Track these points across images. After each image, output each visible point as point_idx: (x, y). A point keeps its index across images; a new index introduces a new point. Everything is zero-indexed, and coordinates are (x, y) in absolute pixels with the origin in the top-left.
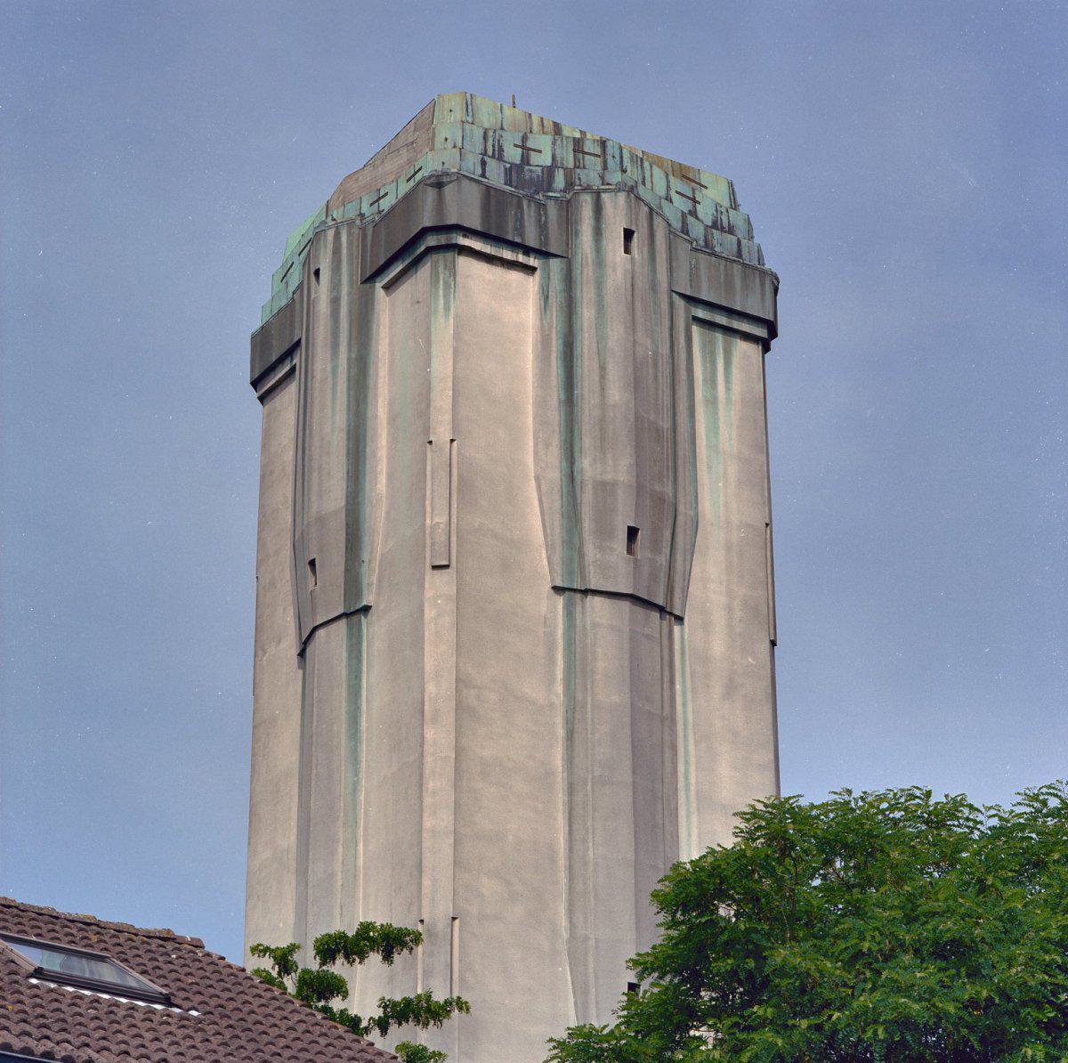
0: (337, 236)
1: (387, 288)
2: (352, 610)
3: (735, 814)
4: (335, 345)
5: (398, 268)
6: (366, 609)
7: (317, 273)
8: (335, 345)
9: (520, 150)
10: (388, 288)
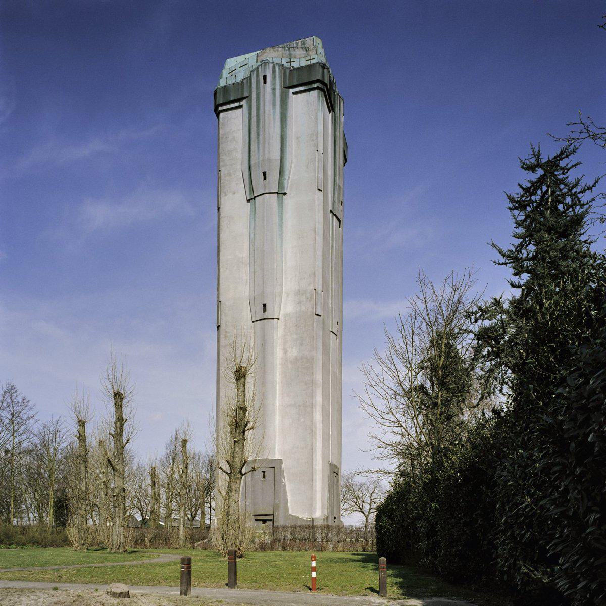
1: (294, 94)
4: (274, 105)
6: (285, 194)
7: (265, 77)
8: (274, 105)
10: (294, 94)
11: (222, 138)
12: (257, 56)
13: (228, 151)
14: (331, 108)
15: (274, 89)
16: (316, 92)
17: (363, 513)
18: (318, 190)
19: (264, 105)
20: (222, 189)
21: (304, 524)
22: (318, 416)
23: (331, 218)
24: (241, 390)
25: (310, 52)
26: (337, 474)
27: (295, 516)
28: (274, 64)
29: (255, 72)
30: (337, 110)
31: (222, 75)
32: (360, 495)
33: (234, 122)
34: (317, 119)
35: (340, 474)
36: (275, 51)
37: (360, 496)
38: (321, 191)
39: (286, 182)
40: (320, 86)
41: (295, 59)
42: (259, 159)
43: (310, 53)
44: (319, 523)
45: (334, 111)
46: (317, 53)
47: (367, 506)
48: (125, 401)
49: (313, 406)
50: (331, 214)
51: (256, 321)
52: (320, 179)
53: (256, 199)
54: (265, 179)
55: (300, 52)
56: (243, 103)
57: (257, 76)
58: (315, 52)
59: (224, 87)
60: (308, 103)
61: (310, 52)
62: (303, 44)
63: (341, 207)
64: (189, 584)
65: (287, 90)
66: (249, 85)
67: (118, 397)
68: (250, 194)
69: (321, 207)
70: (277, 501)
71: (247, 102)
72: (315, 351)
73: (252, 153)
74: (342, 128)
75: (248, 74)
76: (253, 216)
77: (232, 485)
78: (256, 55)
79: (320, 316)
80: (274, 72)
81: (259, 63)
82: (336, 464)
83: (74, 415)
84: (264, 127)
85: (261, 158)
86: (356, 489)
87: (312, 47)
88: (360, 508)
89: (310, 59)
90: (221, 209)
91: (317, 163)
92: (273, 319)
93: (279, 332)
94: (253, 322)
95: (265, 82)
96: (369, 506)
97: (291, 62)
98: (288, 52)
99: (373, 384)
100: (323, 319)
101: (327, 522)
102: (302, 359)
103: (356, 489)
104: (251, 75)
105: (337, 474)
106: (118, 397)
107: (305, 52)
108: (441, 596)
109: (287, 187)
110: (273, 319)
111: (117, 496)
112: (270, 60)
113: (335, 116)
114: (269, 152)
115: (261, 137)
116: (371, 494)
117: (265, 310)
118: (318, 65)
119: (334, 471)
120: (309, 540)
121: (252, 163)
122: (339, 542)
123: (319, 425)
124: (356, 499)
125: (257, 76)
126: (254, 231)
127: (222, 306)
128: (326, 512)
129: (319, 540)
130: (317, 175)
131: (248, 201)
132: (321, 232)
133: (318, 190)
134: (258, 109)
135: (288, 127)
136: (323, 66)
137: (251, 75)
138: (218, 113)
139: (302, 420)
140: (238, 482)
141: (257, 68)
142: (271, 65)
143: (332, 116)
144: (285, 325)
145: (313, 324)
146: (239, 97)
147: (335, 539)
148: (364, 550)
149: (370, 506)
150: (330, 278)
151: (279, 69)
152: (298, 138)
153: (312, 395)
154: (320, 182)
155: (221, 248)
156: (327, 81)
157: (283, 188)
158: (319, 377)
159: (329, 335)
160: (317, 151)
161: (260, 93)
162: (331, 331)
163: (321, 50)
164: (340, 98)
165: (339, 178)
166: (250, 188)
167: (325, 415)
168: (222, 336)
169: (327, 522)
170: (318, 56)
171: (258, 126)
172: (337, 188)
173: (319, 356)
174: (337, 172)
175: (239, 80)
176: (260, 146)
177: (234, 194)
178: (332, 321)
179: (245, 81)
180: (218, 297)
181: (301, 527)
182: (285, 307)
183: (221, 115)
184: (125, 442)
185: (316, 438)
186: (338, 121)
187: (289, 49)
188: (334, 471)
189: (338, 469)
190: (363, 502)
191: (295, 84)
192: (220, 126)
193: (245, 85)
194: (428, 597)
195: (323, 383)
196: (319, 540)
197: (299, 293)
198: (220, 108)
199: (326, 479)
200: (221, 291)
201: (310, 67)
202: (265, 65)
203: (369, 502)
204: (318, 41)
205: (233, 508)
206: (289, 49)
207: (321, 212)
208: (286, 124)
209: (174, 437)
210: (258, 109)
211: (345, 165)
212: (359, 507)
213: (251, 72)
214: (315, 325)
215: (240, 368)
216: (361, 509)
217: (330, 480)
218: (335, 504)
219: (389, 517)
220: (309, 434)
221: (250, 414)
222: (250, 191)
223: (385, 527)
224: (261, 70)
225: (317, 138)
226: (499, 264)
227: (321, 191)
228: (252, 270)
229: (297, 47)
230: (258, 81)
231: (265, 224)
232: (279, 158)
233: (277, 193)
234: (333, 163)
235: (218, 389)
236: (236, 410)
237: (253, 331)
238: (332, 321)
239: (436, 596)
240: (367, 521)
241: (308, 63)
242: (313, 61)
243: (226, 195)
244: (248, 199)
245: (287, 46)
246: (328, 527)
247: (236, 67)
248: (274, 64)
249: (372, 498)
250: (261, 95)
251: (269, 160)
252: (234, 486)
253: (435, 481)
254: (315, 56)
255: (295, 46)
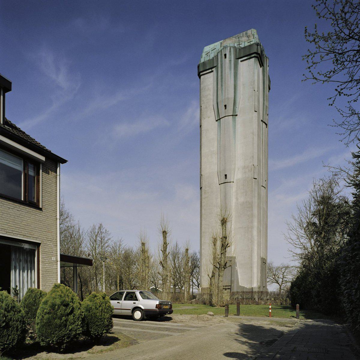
0: (230, 49)
1: (241, 61)
2: (234, 115)
3: (143, 244)
4: (230, 69)
5: (246, 58)
6: (236, 115)
7: (225, 55)
8: (230, 69)
9: (348, 146)
10: (241, 61)
11: (202, 89)
12: (221, 44)
13: (205, 96)
14: (262, 65)
15: (230, 61)
16: (253, 59)
17: (278, 283)
18: (255, 111)
19: (225, 70)
20: (202, 116)
21: (247, 290)
22: (255, 233)
23: (262, 124)
24: (224, 229)
25: (250, 38)
26: (265, 263)
27: (243, 286)
28: (230, 47)
29: (220, 52)
30: (265, 65)
31: (202, 56)
32: (277, 273)
33: (209, 79)
34: (254, 73)
35: (266, 263)
36: (231, 40)
37: (276, 274)
38: (256, 112)
39: (237, 109)
40: (256, 56)
41: (242, 43)
42: (222, 98)
43: (250, 38)
44: (256, 290)
45: (263, 66)
46: (254, 38)
47: (281, 280)
48: (168, 235)
49: (252, 228)
50: (262, 122)
51: (221, 184)
52: (256, 105)
53: (221, 119)
54: (226, 108)
55: (244, 39)
56: (214, 69)
57: (221, 55)
58: (253, 37)
59: (203, 62)
60: (249, 65)
61: (250, 38)
62: (246, 34)
63: (267, 117)
64: (228, 313)
65: (237, 60)
66: (217, 59)
67: (164, 233)
68: (218, 117)
69: (257, 120)
70: (233, 279)
71: (216, 69)
72: (253, 198)
73: (219, 95)
74: (267, 73)
75: (216, 54)
76: (219, 129)
77: (220, 273)
78: (220, 44)
79: (256, 179)
80: (230, 51)
81: (222, 48)
82: (264, 258)
83: (140, 241)
84: (225, 81)
85: (223, 98)
86: (274, 270)
87: (251, 35)
88: (277, 281)
89: (250, 42)
90: (202, 126)
91: (254, 97)
92: (230, 182)
93: (233, 189)
94: (220, 184)
95: (225, 57)
96: (281, 280)
97: (239, 44)
98: (238, 39)
99: (291, 229)
100: (258, 181)
101: (260, 289)
102: (246, 203)
103: (274, 270)
104: (218, 54)
105: (265, 263)
106: (164, 233)
107: (247, 38)
108: (321, 319)
109: (238, 111)
110: (230, 182)
111: (164, 279)
112: (228, 45)
113: (264, 69)
114: (228, 95)
115: (223, 87)
116: (283, 273)
117: (226, 178)
118: (254, 45)
119: (264, 261)
120: (251, 299)
121: (219, 101)
122: (267, 300)
123: (256, 238)
124: (274, 276)
125: (221, 55)
126: (219, 137)
127: (203, 177)
128: (259, 284)
129: (257, 299)
130: (254, 103)
131: (217, 121)
132: (257, 133)
133: (255, 111)
134: (222, 72)
135: (238, 80)
136: (258, 45)
137: (218, 54)
138: (200, 77)
139: (247, 235)
140: (223, 272)
141: (221, 51)
142: (229, 48)
143: (262, 69)
144: (237, 185)
145: (252, 184)
146: (212, 66)
147: (265, 298)
148: (281, 304)
149: (283, 279)
150: (262, 157)
151: (233, 49)
152: (243, 85)
153: (252, 222)
154: (256, 107)
155: (202, 147)
156: (259, 52)
157: (235, 112)
158: (255, 212)
159: (261, 188)
160: (254, 90)
161: (223, 63)
162: (262, 186)
163: (256, 36)
164: (267, 57)
165: (266, 102)
166: (217, 114)
167: (259, 231)
168: (203, 193)
169: (260, 289)
170: (254, 40)
171: (222, 81)
172: (265, 107)
173: (256, 200)
174: (265, 98)
175: (211, 58)
176: (223, 91)
177: (209, 117)
178: (263, 180)
179: (214, 58)
180: (201, 172)
181: (246, 292)
182: (237, 175)
183: (202, 77)
184: (167, 253)
185: (254, 245)
186: (266, 74)
187: (238, 38)
188: (264, 261)
189: (266, 260)
190: (278, 278)
191: (242, 56)
192: (201, 83)
193: (215, 60)
194: (316, 319)
195: (258, 215)
196: (257, 299)
197: (244, 168)
198: (201, 74)
199: (259, 267)
200: (202, 169)
201: (250, 46)
202: (225, 49)
203: (282, 277)
204: (254, 31)
205: (220, 284)
206: (238, 38)
207: (257, 123)
208: (237, 78)
209: (175, 245)
210: (222, 72)
211: (269, 92)
212: (276, 281)
213: (218, 53)
214: (253, 184)
215: (224, 219)
216: (277, 282)
217: (261, 267)
218: (264, 279)
219: (297, 287)
220: (251, 243)
221: (229, 240)
222: (218, 116)
223: (296, 293)
224: (224, 52)
225: (254, 83)
226: (347, 186)
227: (256, 112)
228: (219, 157)
229: (243, 36)
230: (221, 58)
231: (226, 133)
232: (233, 97)
233: (232, 115)
234: (263, 87)
235: (201, 220)
236: (222, 238)
237: (219, 189)
238: (263, 180)
239: (319, 319)
240: (280, 288)
241: (249, 44)
242: (252, 43)
243: (204, 119)
244: (216, 120)
245: (237, 36)
246: (262, 292)
247: (209, 51)
248: (230, 47)
249: (284, 275)
250: (223, 64)
251: (228, 98)
252: (221, 274)
253: (319, 273)
254: (253, 40)
255: (242, 35)
